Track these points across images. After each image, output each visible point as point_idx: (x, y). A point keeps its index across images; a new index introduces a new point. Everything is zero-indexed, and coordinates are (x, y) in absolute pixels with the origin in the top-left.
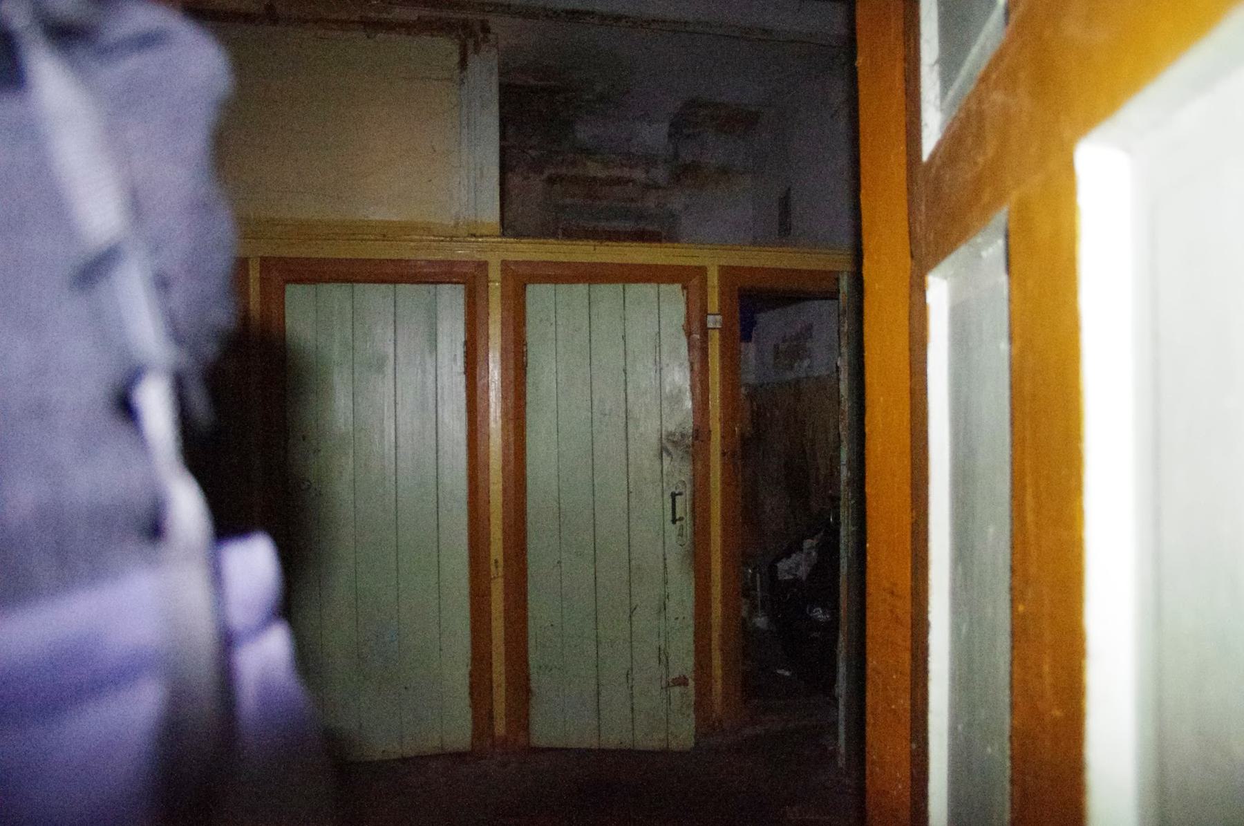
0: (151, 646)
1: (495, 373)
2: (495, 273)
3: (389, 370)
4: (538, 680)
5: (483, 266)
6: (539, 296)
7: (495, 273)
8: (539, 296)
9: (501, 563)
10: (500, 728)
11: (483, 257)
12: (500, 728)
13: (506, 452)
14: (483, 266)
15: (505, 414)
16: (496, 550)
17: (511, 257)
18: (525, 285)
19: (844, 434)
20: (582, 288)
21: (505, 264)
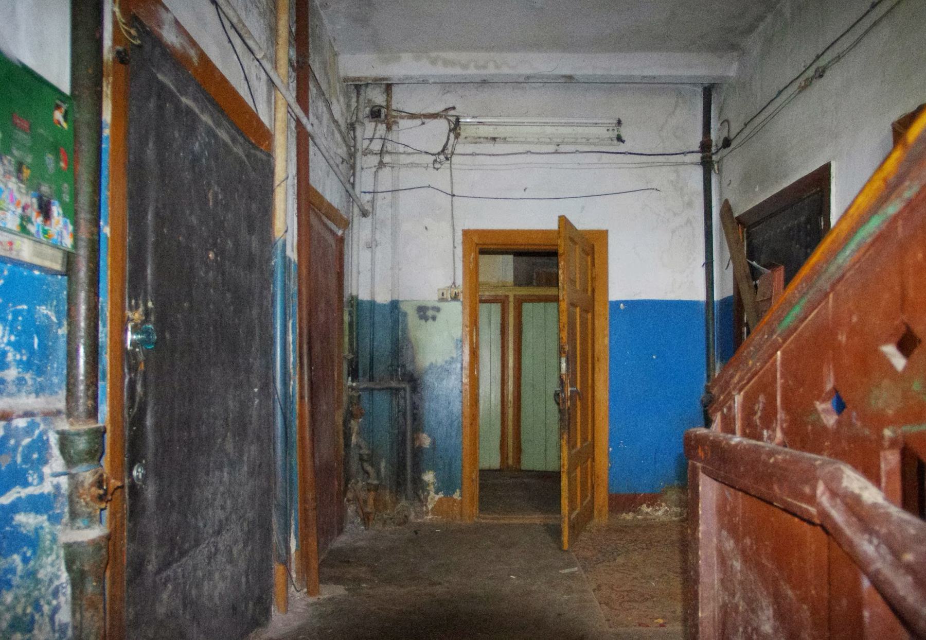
0: (911, 180)
1: (511, 345)
2: (511, 299)
3: (350, 225)
4: (524, 446)
5: (507, 297)
6: (527, 307)
7: (511, 299)
8: (527, 307)
9: (512, 403)
10: (510, 462)
11: (507, 294)
12: (510, 462)
13: (99, 89)
14: (507, 297)
15: (514, 416)
16: (511, 398)
17: (517, 293)
18: (522, 303)
19: (291, 353)
20: (542, 304)
21: (515, 296)
